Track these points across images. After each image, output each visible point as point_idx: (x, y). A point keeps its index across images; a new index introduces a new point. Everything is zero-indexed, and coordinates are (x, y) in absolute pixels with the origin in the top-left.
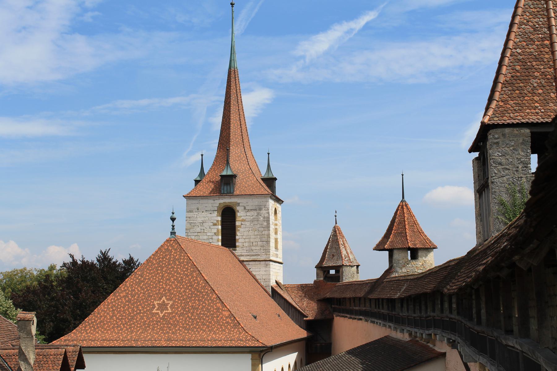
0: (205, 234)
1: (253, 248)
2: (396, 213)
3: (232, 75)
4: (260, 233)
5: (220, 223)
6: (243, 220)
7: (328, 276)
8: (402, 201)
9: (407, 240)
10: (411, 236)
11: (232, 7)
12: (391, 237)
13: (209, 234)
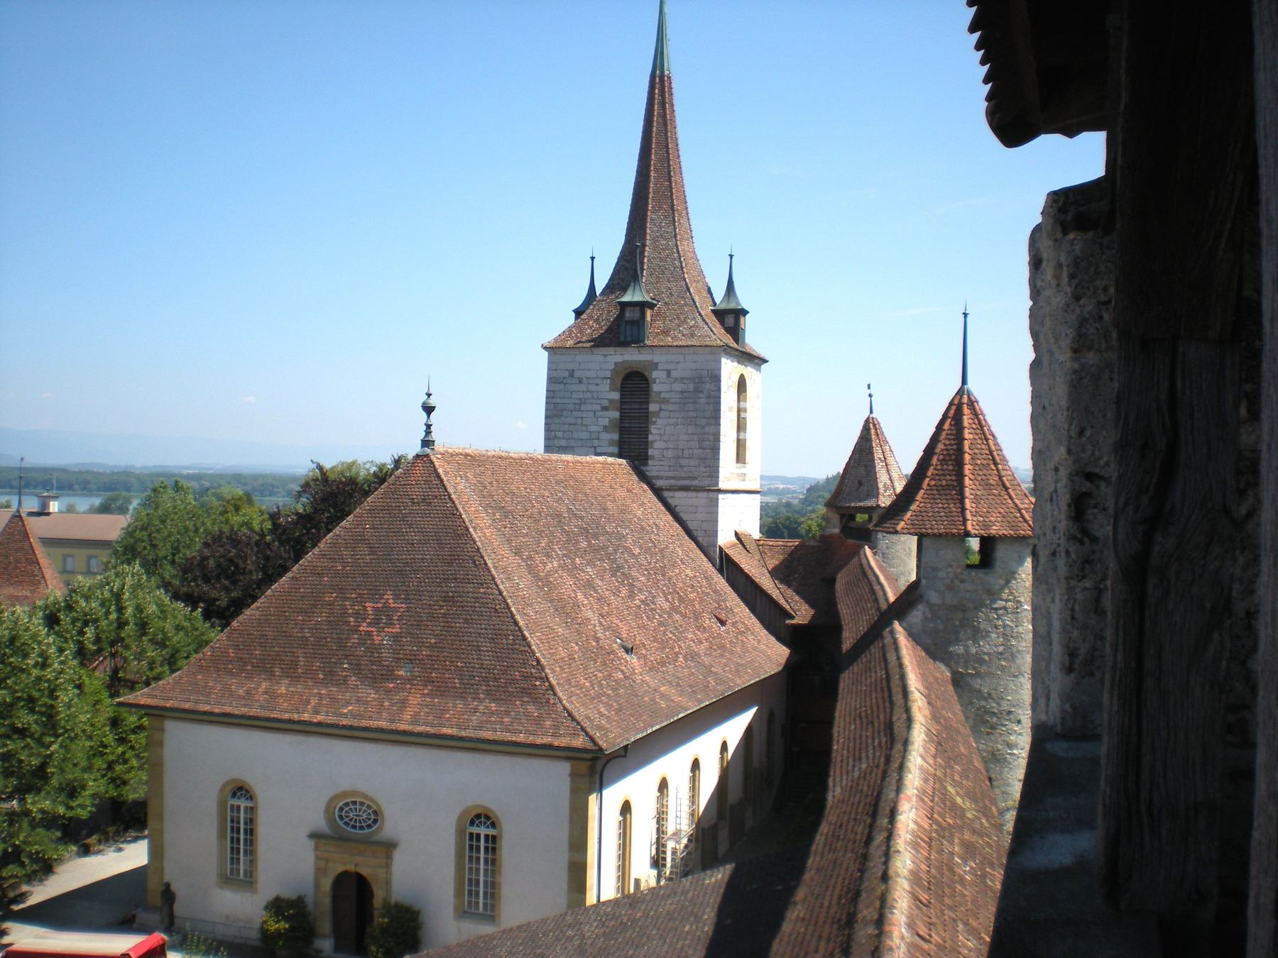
1: (684, 462)
2: (939, 427)
3: (659, 87)
7: (852, 524)
9: (963, 509)
10: (977, 499)
12: (919, 497)
13: (592, 428)
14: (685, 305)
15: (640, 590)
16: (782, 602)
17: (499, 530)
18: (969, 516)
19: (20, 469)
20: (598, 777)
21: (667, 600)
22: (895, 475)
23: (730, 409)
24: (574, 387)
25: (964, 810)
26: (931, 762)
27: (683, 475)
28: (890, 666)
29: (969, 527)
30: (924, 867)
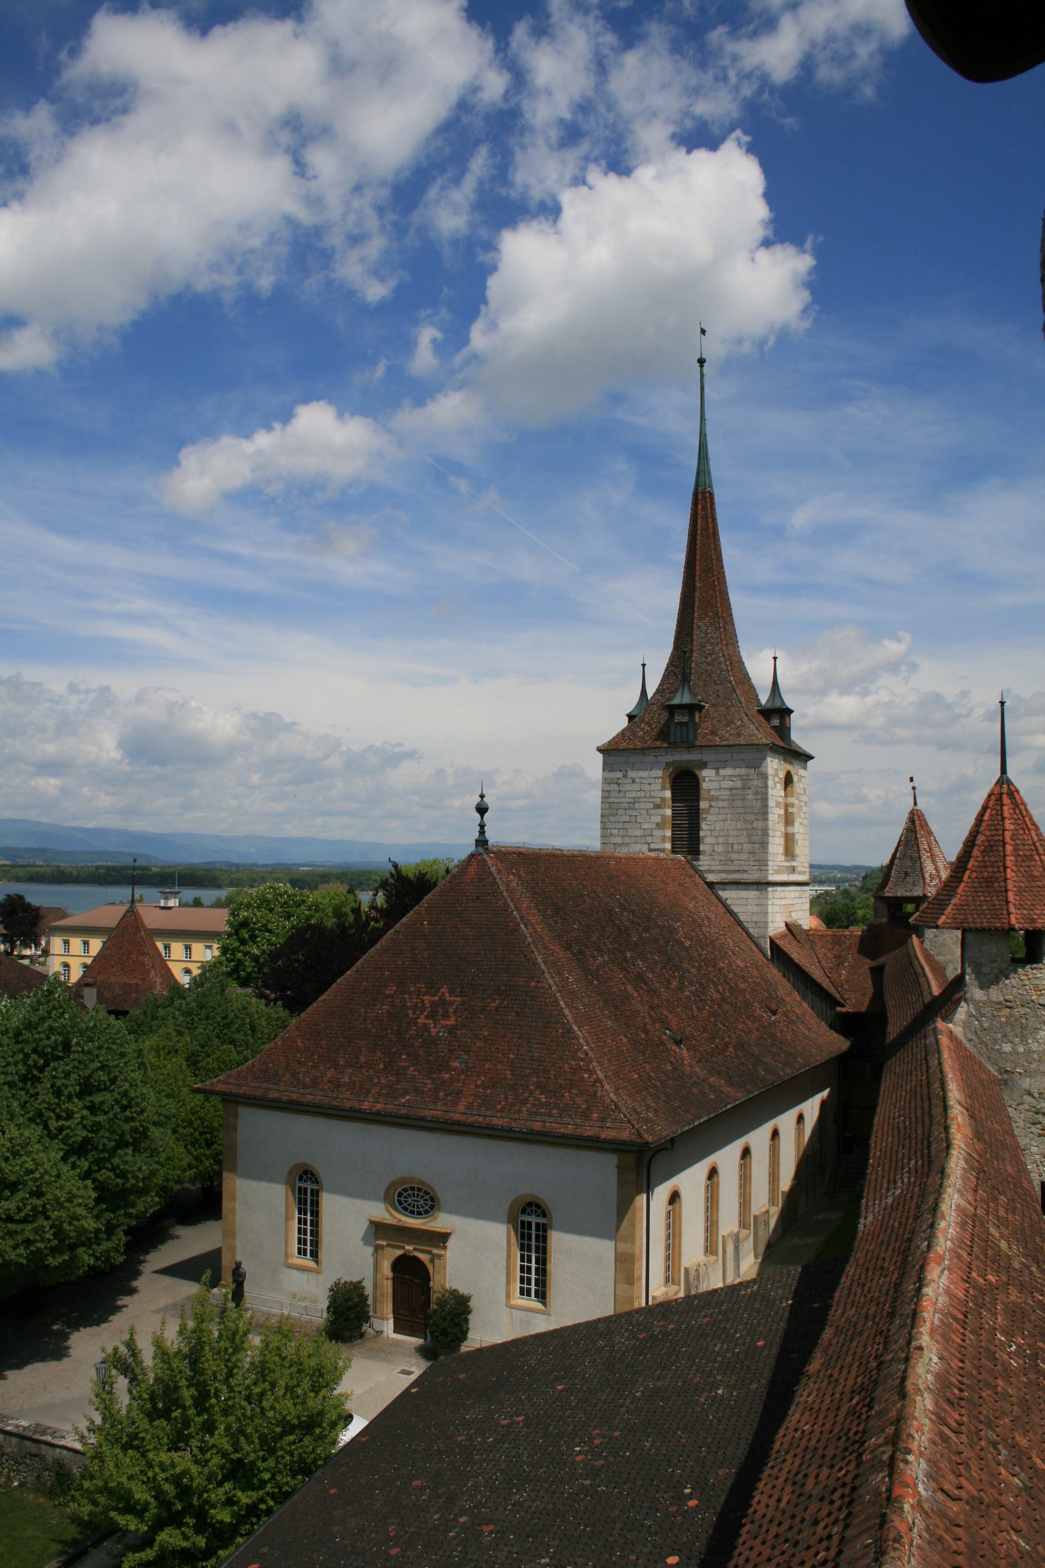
0: (638, 826)
4: (748, 826)
5: (669, 803)
6: (715, 799)
8: (1003, 780)
9: (1007, 902)
10: (1019, 892)
11: (702, 366)
12: (959, 891)
13: (645, 826)
14: (732, 705)
15: (691, 983)
16: (832, 990)
17: (549, 925)
18: (1012, 909)
19: (134, 868)
20: (645, 1168)
21: (718, 991)
22: (940, 865)
23: (778, 804)
24: (628, 787)
25: (1009, 1258)
26: (970, 1198)
27: (733, 868)
28: (931, 1071)
29: (1013, 921)
30: (955, 1364)
